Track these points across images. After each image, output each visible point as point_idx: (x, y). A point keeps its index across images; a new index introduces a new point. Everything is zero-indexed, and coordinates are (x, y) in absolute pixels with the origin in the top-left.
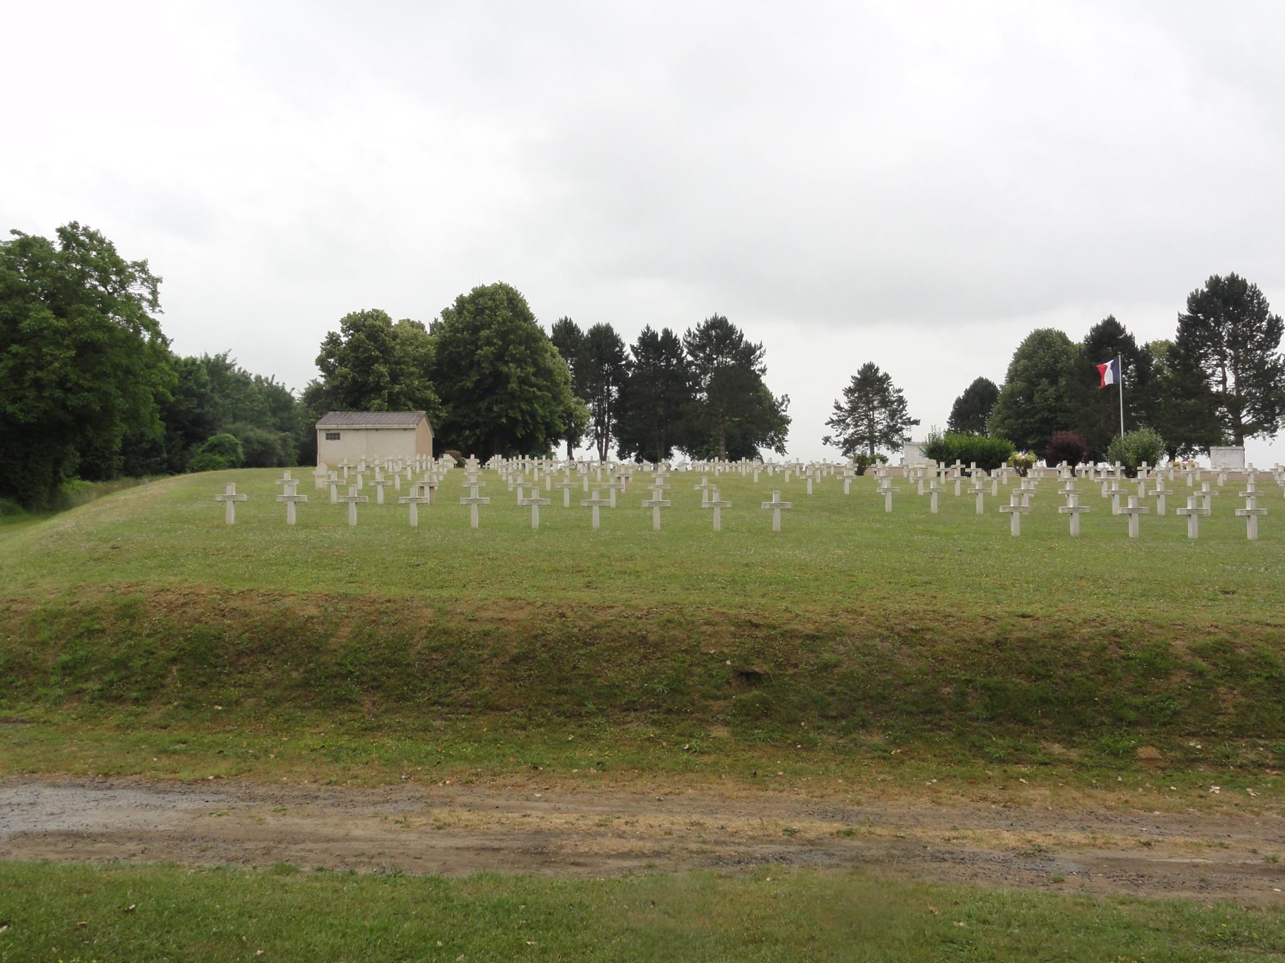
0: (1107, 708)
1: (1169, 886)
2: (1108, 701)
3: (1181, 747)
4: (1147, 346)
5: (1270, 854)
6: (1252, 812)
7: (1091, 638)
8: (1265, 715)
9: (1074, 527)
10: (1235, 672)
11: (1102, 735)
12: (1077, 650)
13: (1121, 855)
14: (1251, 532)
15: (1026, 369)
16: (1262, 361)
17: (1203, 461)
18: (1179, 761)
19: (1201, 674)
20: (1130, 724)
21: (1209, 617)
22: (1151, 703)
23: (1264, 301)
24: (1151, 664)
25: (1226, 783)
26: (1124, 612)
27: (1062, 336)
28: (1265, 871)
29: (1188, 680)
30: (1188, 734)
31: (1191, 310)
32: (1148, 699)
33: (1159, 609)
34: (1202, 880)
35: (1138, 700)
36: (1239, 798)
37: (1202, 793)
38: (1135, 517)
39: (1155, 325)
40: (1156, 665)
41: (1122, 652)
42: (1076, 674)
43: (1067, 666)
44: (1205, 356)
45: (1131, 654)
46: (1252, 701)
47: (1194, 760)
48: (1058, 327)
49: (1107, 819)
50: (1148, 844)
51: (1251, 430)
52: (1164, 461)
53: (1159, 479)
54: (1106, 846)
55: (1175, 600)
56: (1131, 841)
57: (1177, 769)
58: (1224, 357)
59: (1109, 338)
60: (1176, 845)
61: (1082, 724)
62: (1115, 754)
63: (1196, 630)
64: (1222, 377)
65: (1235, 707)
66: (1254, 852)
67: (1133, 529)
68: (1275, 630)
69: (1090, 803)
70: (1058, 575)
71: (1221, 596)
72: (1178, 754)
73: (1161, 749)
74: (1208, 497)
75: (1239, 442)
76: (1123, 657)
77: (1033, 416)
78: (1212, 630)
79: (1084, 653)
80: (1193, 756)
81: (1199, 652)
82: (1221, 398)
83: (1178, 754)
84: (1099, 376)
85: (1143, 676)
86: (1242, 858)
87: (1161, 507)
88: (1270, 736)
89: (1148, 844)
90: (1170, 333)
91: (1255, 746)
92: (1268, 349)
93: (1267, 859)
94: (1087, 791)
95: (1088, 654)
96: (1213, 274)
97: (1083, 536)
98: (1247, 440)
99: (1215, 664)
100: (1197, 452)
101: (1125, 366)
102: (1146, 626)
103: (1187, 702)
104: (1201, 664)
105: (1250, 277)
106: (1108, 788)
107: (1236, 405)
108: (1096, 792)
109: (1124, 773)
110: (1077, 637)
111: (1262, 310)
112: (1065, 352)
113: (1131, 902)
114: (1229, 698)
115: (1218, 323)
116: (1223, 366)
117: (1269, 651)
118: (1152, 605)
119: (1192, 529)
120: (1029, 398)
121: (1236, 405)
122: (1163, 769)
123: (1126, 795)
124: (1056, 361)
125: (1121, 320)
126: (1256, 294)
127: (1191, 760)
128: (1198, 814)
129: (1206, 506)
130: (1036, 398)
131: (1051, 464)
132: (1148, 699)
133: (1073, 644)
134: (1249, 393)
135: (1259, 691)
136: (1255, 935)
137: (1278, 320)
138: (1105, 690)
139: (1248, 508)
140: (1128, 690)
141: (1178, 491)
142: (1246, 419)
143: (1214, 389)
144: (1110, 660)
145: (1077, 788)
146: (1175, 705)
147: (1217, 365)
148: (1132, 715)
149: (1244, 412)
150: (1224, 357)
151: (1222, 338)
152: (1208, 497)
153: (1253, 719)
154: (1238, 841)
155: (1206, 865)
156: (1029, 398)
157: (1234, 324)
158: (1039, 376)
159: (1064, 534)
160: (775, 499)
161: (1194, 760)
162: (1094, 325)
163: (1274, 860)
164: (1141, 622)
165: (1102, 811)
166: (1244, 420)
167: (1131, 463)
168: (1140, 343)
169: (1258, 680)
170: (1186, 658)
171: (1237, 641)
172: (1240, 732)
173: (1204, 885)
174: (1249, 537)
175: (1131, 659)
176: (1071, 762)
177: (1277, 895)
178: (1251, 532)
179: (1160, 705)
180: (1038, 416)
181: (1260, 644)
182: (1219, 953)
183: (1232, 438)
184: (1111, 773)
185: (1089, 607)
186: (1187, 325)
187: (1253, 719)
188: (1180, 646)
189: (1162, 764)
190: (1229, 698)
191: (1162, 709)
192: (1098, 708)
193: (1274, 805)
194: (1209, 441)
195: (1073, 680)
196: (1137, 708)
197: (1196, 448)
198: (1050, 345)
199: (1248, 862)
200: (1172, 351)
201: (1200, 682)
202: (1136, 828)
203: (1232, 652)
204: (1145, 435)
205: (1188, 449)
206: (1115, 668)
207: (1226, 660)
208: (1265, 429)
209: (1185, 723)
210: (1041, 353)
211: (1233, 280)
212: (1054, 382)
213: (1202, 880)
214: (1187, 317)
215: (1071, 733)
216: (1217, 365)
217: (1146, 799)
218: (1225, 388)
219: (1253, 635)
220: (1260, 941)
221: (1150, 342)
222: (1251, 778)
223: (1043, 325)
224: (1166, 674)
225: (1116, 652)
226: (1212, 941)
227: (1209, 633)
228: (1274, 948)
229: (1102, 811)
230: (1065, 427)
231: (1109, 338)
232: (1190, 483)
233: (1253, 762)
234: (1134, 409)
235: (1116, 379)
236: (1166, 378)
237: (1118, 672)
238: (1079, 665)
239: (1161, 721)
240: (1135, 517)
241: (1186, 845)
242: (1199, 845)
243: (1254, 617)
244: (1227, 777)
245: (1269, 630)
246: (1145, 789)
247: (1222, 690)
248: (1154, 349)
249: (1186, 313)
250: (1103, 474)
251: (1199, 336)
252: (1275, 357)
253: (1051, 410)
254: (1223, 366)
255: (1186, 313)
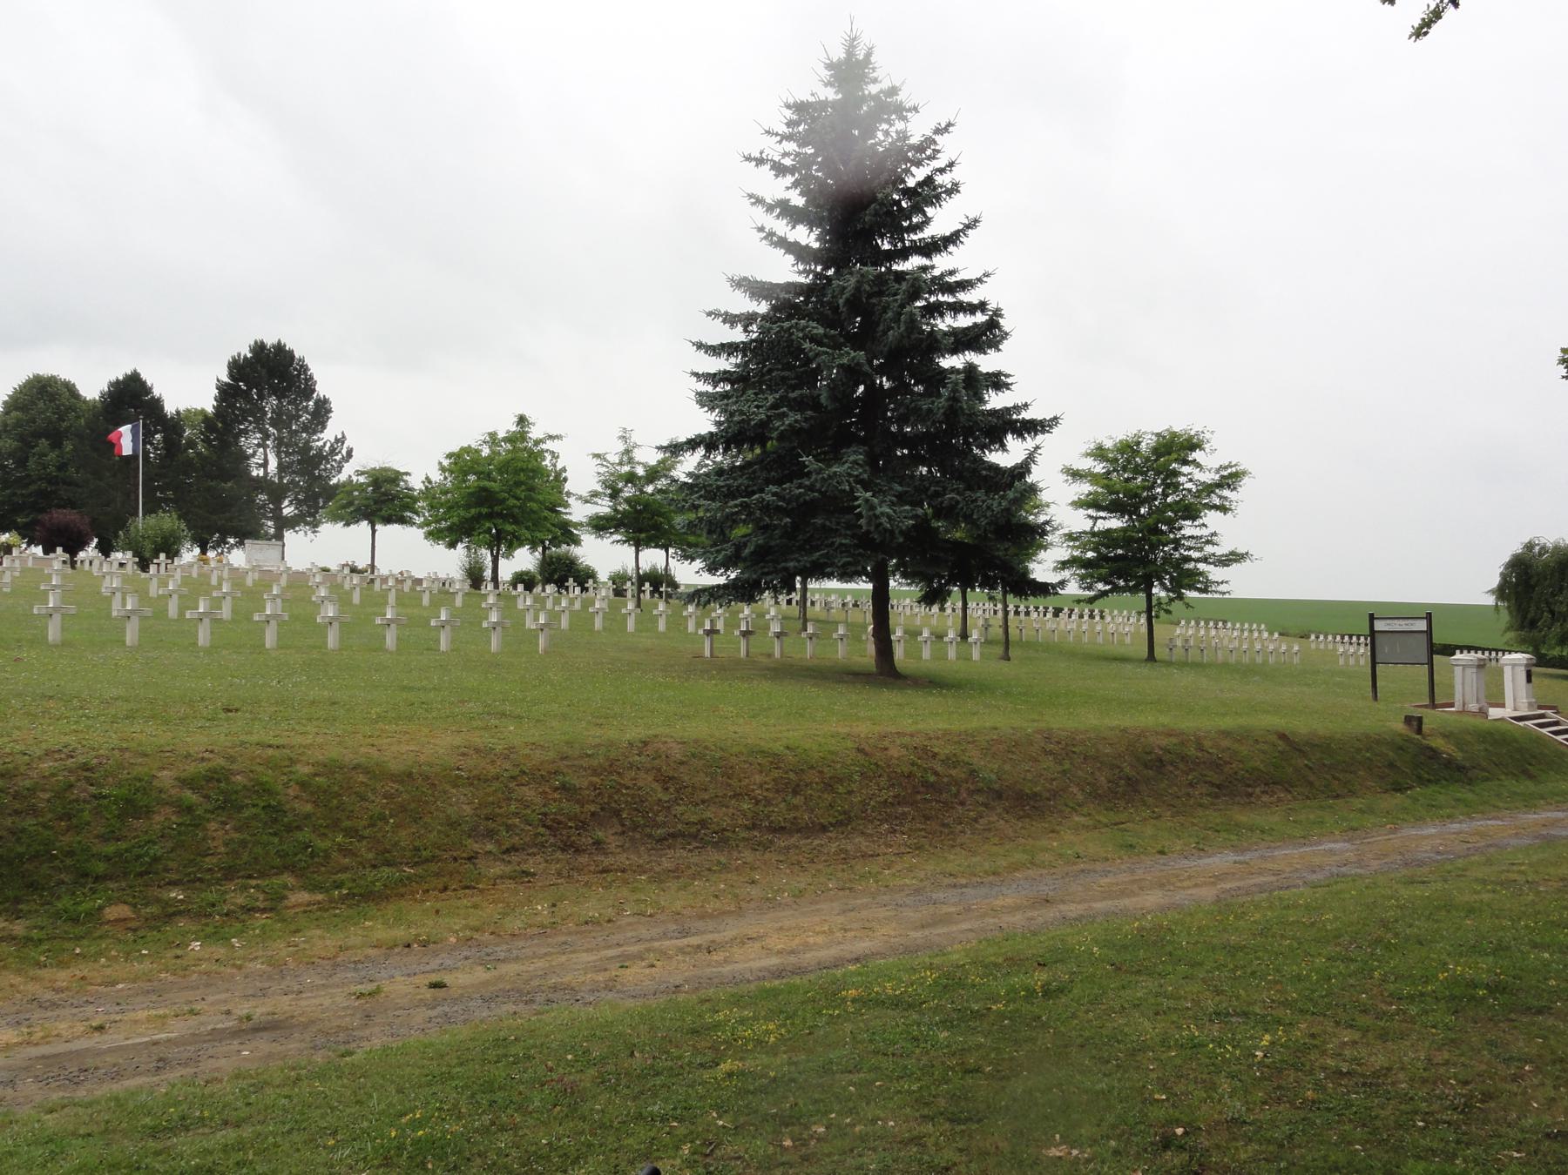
0: (69, 862)
1: (117, 1075)
2: (71, 854)
3: (158, 900)
4: (178, 412)
5: (245, 1012)
6: (234, 965)
7: (53, 775)
8: (259, 850)
9: (53, 632)
10: (228, 804)
11: (59, 898)
12: (32, 790)
13: (61, 1048)
14: (270, 639)
15: (19, 424)
16: (308, 447)
17: (238, 557)
18: (155, 917)
19: (190, 809)
20: (97, 879)
21: (204, 740)
22: (126, 850)
23: (311, 378)
24: (128, 801)
25: (208, 936)
26: (98, 738)
27: (70, 388)
28: (236, 1033)
29: (174, 818)
30: (169, 884)
31: (231, 376)
32: (123, 845)
33: (147, 734)
34: (160, 1060)
35: (110, 849)
36: (220, 951)
37: (179, 952)
38: (135, 619)
39: (188, 389)
40: (135, 804)
41: (92, 789)
42: (29, 822)
43: (17, 812)
44: (245, 432)
45: (105, 792)
46: (246, 836)
47: (175, 914)
48: (64, 374)
49: (54, 1005)
50: (100, 1028)
51: (292, 523)
52: (189, 554)
53: (178, 575)
54: (45, 1039)
55: (166, 722)
56: (80, 1028)
57: (151, 928)
58: (266, 436)
59: (130, 397)
60: (136, 1022)
61: (33, 886)
62: (75, 920)
63: (188, 756)
64: (264, 461)
65: (226, 845)
66: (228, 1013)
67: (131, 635)
68: (276, 753)
69: (32, 988)
70: (19, 695)
71: (223, 715)
72: (153, 909)
73: (135, 906)
74: (229, 598)
75: (279, 536)
76: (94, 796)
77: (26, 486)
78: (207, 755)
79: (41, 795)
80: (171, 910)
81: (187, 783)
82: (262, 484)
83: (153, 909)
84: (113, 446)
85: (118, 817)
86: (214, 1021)
87: (173, 611)
88: (262, 875)
89: (100, 1028)
90: (206, 401)
91: (245, 888)
92: (315, 432)
93: (240, 1019)
94: (31, 973)
95: (47, 796)
96: (259, 338)
97: (64, 644)
98: (288, 535)
99: (207, 797)
100: (232, 547)
101: (148, 435)
102: (127, 755)
103: (170, 844)
104: (190, 796)
105: (300, 348)
106: (62, 965)
107: (277, 493)
108: (45, 973)
109: (85, 942)
110: (34, 774)
111: (308, 390)
112: (72, 408)
113: (63, 1107)
114: (219, 834)
115: (261, 397)
116: (265, 447)
117: (267, 776)
118: (137, 728)
119: (203, 636)
120: (22, 463)
121: (277, 493)
122: (135, 930)
123: (83, 969)
124: (61, 419)
125: (147, 376)
126: (304, 368)
127: (170, 914)
128: (171, 978)
129: (226, 612)
130: (31, 464)
131: (48, 550)
132: (123, 845)
133: (27, 783)
134: (292, 482)
135: (254, 823)
136: (206, 1114)
137: (326, 401)
138: (66, 839)
139: (443, 618)
140: (97, 837)
141: (196, 587)
142: (288, 510)
143: (254, 473)
144: (77, 801)
145: (19, 972)
146: (156, 850)
147: (259, 445)
148: (101, 867)
149: (286, 503)
150: (266, 436)
151: (265, 413)
152: (229, 598)
153: (245, 857)
154: (212, 1004)
155: (169, 1040)
156: (22, 463)
157: (279, 399)
158: (37, 435)
159: (39, 641)
160: (926, 634)
161: (175, 914)
162: (113, 379)
163: (249, 1018)
164: (121, 750)
165: (49, 995)
166: (286, 511)
167: (147, 555)
168: (170, 408)
169: (254, 810)
170: (173, 792)
171: (234, 767)
172: (229, 873)
173: (162, 1064)
174: (268, 646)
175: (105, 797)
176: (12, 938)
177: (245, 1059)
178: (270, 639)
179: (136, 851)
180: (33, 488)
181: (260, 769)
182: (160, 1146)
183: (272, 531)
184: (67, 945)
185: (54, 735)
186: (226, 393)
187: (245, 857)
188: (166, 777)
189: (133, 925)
190: (219, 834)
191: (138, 857)
192: (57, 862)
193: (260, 953)
194: (246, 533)
195: (23, 830)
196: (108, 858)
197: (232, 541)
198: (53, 397)
199: (220, 1026)
200: (208, 423)
201: (187, 819)
202: (90, 1009)
203: (227, 779)
204: (167, 521)
205: (222, 542)
206: (82, 811)
207: (220, 791)
208: (307, 523)
209: (167, 870)
210: (41, 404)
211: (280, 348)
212: (56, 444)
213: (160, 1060)
214: (227, 384)
215: (17, 901)
216: (259, 445)
217: (108, 971)
218: (266, 473)
219: (253, 758)
220: (211, 1119)
221: (181, 409)
222: (239, 925)
223: (46, 371)
224: (148, 813)
225: (85, 790)
226: (154, 1133)
227: (203, 759)
228: (226, 1123)
229: (49, 995)
230: (71, 504)
231: (130, 397)
232: (214, 581)
233: (242, 907)
234: (162, 489)
235: (135, 449)
236: (199, 454)
237: (86, 815)
238: (34, 811)
239: (135, 872)
240: (135, 619)
241: (149, 1019)
242: (165, 1016)
243: (255, 738)
244: (210, 930)
245: (270, 752)
246: (108, 959)
247: (213, 826)
248: (187, 417)
249: (226, 380)
250: (106, 570)
251: (240, 409)
252: (320, 443)
253: (51, 480)
254: (265, 447)
255: (226, 380)
